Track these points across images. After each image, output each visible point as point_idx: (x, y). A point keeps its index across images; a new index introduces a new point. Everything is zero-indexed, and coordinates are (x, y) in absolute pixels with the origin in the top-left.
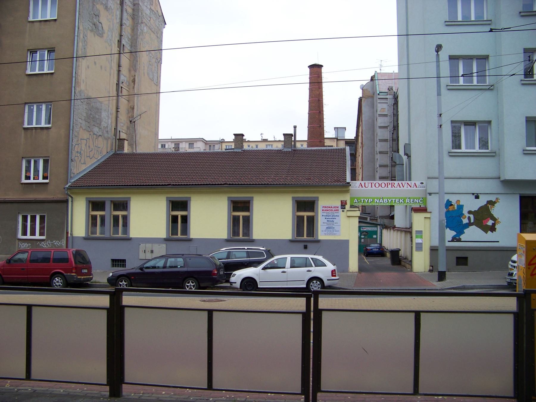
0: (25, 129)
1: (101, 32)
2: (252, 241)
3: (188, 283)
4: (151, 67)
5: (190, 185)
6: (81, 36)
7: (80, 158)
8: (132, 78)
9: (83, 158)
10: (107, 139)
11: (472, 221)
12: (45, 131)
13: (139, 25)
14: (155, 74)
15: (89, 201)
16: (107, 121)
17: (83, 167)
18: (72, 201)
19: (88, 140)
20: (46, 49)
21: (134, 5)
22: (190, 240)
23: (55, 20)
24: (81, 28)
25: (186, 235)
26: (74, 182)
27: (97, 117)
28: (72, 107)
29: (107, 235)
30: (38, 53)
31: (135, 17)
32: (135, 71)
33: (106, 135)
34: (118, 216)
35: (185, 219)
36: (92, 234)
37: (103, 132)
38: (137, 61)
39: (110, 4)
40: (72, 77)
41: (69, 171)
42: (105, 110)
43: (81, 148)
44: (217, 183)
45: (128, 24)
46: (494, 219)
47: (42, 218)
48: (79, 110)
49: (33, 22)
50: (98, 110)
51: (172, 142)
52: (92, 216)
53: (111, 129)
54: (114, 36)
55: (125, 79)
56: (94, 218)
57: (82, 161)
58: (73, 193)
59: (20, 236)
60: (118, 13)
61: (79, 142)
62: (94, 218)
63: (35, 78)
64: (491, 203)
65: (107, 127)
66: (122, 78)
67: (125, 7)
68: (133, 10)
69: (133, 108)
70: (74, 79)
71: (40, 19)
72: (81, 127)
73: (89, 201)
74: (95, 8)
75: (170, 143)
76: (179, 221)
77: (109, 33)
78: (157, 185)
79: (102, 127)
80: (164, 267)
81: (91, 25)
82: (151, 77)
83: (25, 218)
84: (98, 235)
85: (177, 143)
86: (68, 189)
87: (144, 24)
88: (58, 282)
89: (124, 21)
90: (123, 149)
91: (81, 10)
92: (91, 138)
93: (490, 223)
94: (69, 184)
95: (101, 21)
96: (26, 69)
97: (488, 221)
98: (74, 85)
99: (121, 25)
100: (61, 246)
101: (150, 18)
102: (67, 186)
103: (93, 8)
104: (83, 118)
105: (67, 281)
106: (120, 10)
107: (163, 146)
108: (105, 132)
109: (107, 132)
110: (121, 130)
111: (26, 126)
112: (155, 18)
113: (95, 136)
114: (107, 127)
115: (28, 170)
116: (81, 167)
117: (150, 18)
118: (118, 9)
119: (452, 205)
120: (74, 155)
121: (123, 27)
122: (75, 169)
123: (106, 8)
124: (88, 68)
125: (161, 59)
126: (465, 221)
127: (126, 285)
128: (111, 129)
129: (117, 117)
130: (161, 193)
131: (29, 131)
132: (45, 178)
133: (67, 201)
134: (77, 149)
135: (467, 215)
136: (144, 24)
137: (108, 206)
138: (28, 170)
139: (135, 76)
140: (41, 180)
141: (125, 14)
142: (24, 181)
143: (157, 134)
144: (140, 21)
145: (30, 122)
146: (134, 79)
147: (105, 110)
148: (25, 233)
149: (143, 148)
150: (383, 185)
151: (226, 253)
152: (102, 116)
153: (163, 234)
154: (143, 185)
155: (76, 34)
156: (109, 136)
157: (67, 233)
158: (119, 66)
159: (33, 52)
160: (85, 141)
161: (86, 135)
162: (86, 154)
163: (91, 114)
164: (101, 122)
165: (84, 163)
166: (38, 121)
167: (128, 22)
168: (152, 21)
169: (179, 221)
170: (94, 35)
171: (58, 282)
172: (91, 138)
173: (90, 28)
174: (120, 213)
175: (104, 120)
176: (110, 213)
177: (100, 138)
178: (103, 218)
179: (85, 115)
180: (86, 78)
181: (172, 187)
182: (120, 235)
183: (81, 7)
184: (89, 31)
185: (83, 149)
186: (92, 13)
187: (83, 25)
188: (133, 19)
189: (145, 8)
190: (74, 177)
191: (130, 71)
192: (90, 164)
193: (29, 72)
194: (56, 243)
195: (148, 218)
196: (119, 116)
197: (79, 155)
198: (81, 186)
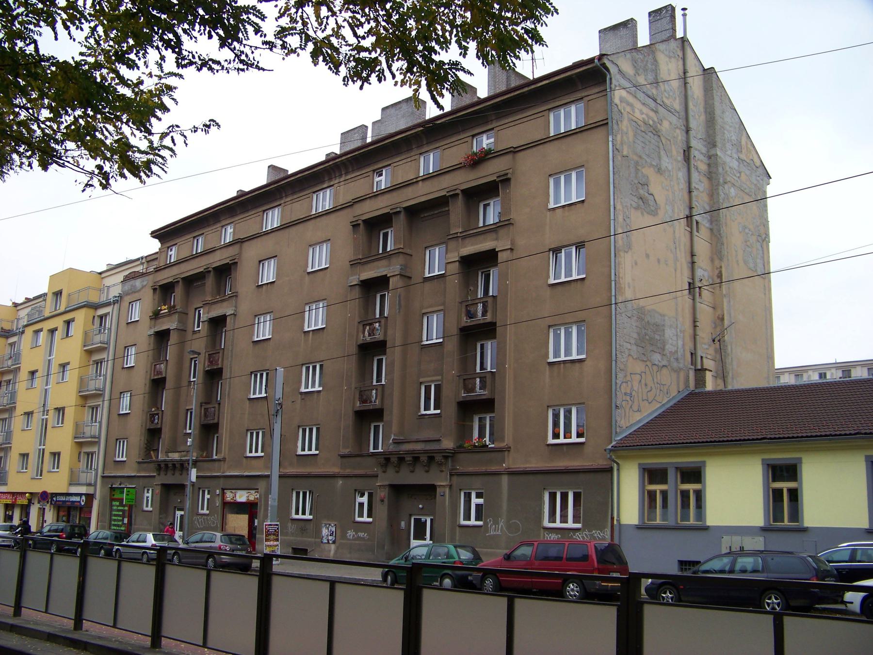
0: (551, 364)
1: (653, 209)
3: (770, 599)
4: (749, 250)
5: (798, 437)
6: (620, 218)
7: (630, 402)
8: (717, 272)
9: (636, 403)
10: (677, 371)
12: (577, 365)
13: (721, 188)
14: (758, 261)
15: (644, 469)
16: (675, 343)
17: (637, 417)
18: (618, 470)
19: (643, 374)
20: (572, 245)
21: (710, 157)
22: (805, 530)
23: (583, 201)
24: (619, 207)
25: (798, 522)
26: (621, 440)
27: (657, 337)
28: (614, 326)
29: (670, 522)
30: (563, 251)
31: (712, 175)
32: (721, 259)
33: (675, 365)
34: (655, 492)
35: (794, 495)
36: (648, 520)
37: (669, 361)
38: (723, 244)
39: (666, 163)
40: (611, 281)
41: (613, 423)
42: (671, 326)
43: (632, 386)
44: (843, 433)
45: (701, 189)
47: (577, 496)
48: (626, 329)
49: (554, 209)
50: (659, 328)
51: (837, 368)
52: (649, 492)
53: (684, 355)
54: (676, 210)
55: (706, 274)
56: (652, 495)
57: (635, 408)
58: (618, 457)
59: (546, 523)
60: (682, 175)
61: (628, 378)
62: (652, 495)
63: (560, 288)
65: (676, 352)
66: (699, 273)
67: (692, 162)
68: (709, 165)
69: (722, 319)
70: (613, 283)
71: (563, 203)
72: (629, 355)
73: (644, 469)
74: (640, 174)
75: (833, 371)
76: (784, 499)
77: (668, 208)
78: (744, 440)
79: (667, 352)
80: (731, 571)
81: (636, 200)
82: (751, 265)
83: (553, 496)
84: (658, 521)
85: (798, 371)
86: (611, 450)
87: (730, 185)
88: (573, 590)
89: (693, 185)
90: (704, 385)
91: (617, 182)
92: (648, 372)
94: (614, 443)
95: (651, 191)
96: (548, 277)
98: (613, 294)
99: (690, 192)
100: (604, 539)
101: (740, 173)
102: (610, 447)
103: (637, 173)
104: (633, 341)
105: (585, 589)
106: (685, 170)
107: (822, 375)
108: (672, 359)
109: (677, 359)
110: (704, 355)
111: (551, 359)
112: (748, 172)
113: (655, 368)
114: (676, 352)
115: (556, 424)
116: (632, 417)
117: (740, 173)
118: (679, 169)
120: (619, 399)
121: (694, 194)
122: (623, 421)
123: (659, 171)
124: (636, 264)
125: (767, 235)
127: (672, 598)
128: (684, 355)
129: (695, 335)
130: (753, 453)
131: (556, 366)
132: (579, 435)
133: (610, 470)
134: (624, 388)
136: (730, 185)
137: (671, 475)
138: (556, 424)
139: (721, 267)
140: (574, 439)
141: (695, 176)
142: (551, 441)
143: (770, 357)
144: (721, 181)
145: (557, 353)
146: (721, 272)
147: (671, 326)
148: (552, 519)
149: (744, 379)
151: (849, 551)
152: (667, 336)
153: (758, 520)
154: (723, 441)
155: (612, 217)
156: (681, 366)
157: (612, 518)
158: (692, 255)
159: (556, 251)
160: (638, 377)
161: (639, 367)
162: (640, 395)
163: (646, 334)
164: (664, 346)
165: (638, 411)
166: (568, 352)
167: (700, 184)
168: (743, 177)
169: (784, 499)
170: (642, 214)
171: (573, 590)
172: (648, 372)
173: (635, 205)
174: (691, 487)
175: (670, 341)
176: (677, 485)
177: (664, 371)
178: (664, 494)
179: (635, 336)
180: (633, 280)
181: (769, 443)
182: (692, 521)
183: (616, 176)
184: (633, 210)
185: (635, 388)
186: (636, 182)
187: (622, 204)
188: (710, 179)
189: (728, 159)
190: (621, 433)
191: (712, 260)
192: (650, 411)
193: (552, 281)
194: (596, 533)
195: (733, 494)
196: (698, 332)
197: (628, 398)
198: (630, 447)
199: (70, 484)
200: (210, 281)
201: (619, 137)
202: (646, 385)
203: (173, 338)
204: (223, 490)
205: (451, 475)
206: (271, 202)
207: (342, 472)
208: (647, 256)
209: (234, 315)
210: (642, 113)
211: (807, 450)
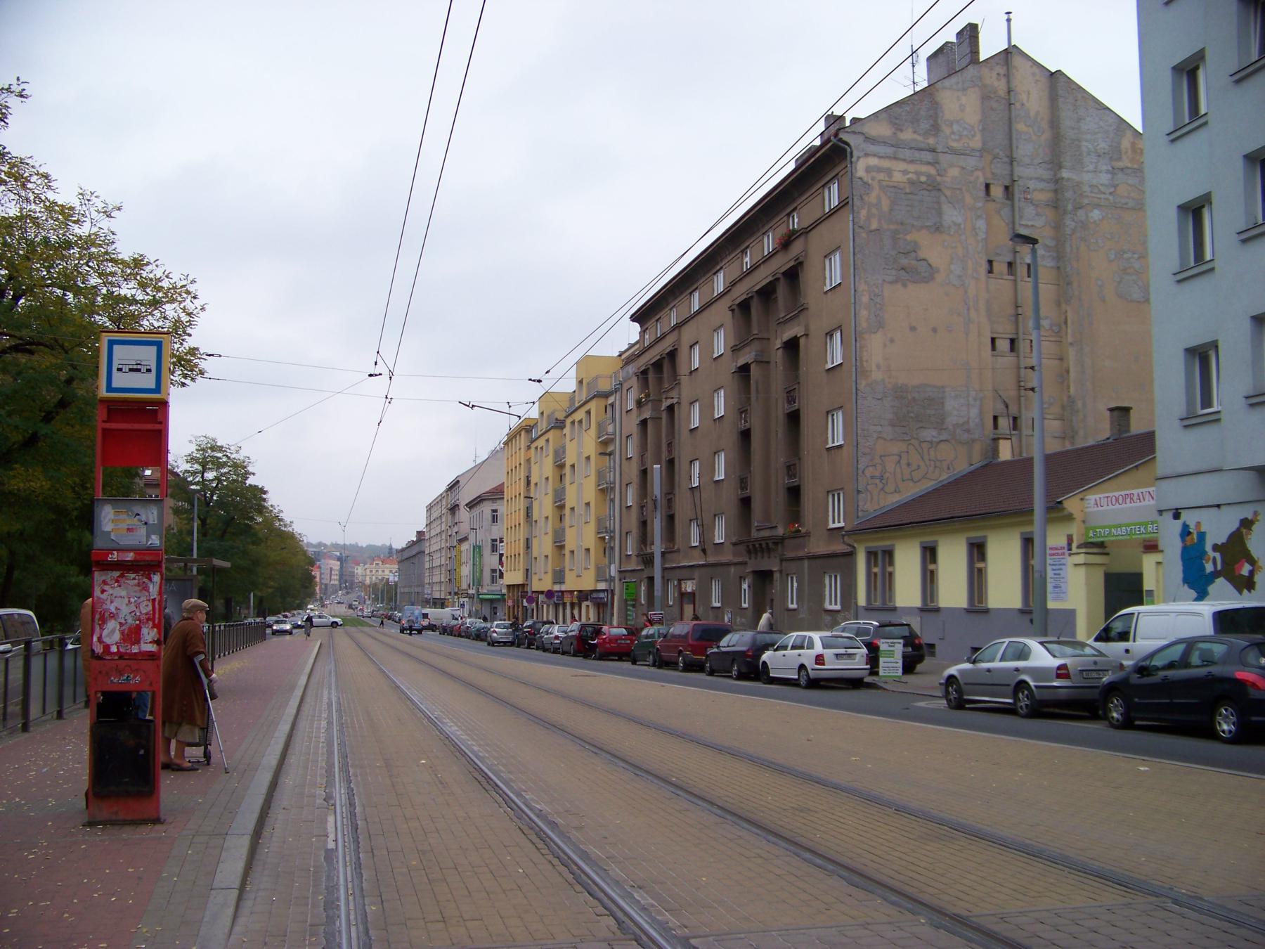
2: (894, 609)
11: (1219, 567)
46: (1252, 562)
64: (1246, 524)
65: (968, 422)
68: (1056, 191)
69: (1068, 372)
93: (1245, 570)
97: (1242, 566)
113: (925, 445)
119: (1189, 533)
126: (1209, 568)
135: (1211, 554)
150: (1104, 502)
183: (858, 256)
191: (1058, 304)
197: (877, 481)
199: (598, 581)
200: (782, 291)
201: (864, 213)
202: (909, 465)
203: (754, 370)
204: (680, 581)
205: (782, 560)
206: (808, 189)
207: (736, 560)
208: (913, 329)
209: (807, 335)
210: (905, 172)
211: (993, 528)
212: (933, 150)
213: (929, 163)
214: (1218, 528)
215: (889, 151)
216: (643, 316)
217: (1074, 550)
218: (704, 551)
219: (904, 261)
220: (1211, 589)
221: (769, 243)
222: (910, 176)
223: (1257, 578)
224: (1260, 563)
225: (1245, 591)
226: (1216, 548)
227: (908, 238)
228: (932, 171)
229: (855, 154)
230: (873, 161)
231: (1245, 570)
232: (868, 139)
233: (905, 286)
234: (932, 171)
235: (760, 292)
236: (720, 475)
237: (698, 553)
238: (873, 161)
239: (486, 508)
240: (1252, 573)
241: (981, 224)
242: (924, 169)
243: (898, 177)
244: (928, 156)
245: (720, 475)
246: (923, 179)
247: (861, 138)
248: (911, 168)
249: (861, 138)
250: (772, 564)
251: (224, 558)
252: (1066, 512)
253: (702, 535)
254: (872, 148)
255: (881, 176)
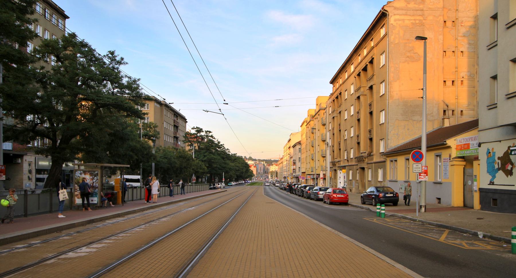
46: (512, 164)
93: (509, 167)
119: (490, 153)
135: (497, 161)
201: (392, 37)
212: (422, 10)
213: (420, 15)
214: (500, 150)
215: (404, 12)
216: (333, 82)
217: (451, 160)
218: (348, 161)
219: (408, 54)
220: (497, 175)
221: (365, 52)
222: (412, 21)
223: (513, 171)
224: (515, 165)
225: (509, 176)
226: (499, 158)
227: (410, 45)
228: (421, 18)
229: (390, 15)
230: (397, 17)
231: (509, 167)
232: (395, 8)
233: (408, 63)
234: (421, 18)
235: (363, 70)
236: (352, 135)
237: (346, 161)
238: (397, 17)
239: (298, 147)
240: (512, 169)
241: (441, 37)
242: (418, 18)
243: (407, 22)
244: (420, 13)
245: (352, 135)
246: (417, 22)
247: (393, 8)
248: (412, 18)
249: (393, 8)
250: (364, 165)
251: (57, 142)
252: (448, 145)
253: (347, 156)
254: (396, 12)
255: (400, 22)
